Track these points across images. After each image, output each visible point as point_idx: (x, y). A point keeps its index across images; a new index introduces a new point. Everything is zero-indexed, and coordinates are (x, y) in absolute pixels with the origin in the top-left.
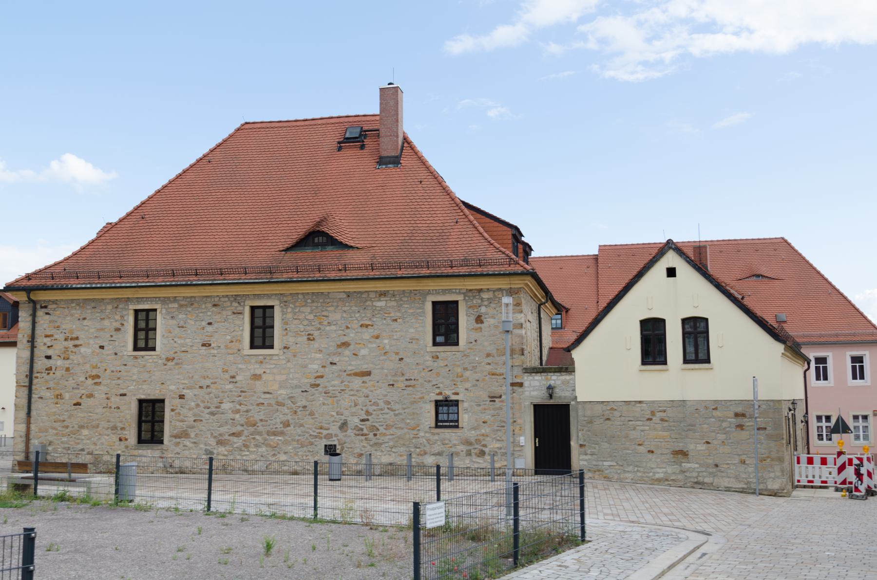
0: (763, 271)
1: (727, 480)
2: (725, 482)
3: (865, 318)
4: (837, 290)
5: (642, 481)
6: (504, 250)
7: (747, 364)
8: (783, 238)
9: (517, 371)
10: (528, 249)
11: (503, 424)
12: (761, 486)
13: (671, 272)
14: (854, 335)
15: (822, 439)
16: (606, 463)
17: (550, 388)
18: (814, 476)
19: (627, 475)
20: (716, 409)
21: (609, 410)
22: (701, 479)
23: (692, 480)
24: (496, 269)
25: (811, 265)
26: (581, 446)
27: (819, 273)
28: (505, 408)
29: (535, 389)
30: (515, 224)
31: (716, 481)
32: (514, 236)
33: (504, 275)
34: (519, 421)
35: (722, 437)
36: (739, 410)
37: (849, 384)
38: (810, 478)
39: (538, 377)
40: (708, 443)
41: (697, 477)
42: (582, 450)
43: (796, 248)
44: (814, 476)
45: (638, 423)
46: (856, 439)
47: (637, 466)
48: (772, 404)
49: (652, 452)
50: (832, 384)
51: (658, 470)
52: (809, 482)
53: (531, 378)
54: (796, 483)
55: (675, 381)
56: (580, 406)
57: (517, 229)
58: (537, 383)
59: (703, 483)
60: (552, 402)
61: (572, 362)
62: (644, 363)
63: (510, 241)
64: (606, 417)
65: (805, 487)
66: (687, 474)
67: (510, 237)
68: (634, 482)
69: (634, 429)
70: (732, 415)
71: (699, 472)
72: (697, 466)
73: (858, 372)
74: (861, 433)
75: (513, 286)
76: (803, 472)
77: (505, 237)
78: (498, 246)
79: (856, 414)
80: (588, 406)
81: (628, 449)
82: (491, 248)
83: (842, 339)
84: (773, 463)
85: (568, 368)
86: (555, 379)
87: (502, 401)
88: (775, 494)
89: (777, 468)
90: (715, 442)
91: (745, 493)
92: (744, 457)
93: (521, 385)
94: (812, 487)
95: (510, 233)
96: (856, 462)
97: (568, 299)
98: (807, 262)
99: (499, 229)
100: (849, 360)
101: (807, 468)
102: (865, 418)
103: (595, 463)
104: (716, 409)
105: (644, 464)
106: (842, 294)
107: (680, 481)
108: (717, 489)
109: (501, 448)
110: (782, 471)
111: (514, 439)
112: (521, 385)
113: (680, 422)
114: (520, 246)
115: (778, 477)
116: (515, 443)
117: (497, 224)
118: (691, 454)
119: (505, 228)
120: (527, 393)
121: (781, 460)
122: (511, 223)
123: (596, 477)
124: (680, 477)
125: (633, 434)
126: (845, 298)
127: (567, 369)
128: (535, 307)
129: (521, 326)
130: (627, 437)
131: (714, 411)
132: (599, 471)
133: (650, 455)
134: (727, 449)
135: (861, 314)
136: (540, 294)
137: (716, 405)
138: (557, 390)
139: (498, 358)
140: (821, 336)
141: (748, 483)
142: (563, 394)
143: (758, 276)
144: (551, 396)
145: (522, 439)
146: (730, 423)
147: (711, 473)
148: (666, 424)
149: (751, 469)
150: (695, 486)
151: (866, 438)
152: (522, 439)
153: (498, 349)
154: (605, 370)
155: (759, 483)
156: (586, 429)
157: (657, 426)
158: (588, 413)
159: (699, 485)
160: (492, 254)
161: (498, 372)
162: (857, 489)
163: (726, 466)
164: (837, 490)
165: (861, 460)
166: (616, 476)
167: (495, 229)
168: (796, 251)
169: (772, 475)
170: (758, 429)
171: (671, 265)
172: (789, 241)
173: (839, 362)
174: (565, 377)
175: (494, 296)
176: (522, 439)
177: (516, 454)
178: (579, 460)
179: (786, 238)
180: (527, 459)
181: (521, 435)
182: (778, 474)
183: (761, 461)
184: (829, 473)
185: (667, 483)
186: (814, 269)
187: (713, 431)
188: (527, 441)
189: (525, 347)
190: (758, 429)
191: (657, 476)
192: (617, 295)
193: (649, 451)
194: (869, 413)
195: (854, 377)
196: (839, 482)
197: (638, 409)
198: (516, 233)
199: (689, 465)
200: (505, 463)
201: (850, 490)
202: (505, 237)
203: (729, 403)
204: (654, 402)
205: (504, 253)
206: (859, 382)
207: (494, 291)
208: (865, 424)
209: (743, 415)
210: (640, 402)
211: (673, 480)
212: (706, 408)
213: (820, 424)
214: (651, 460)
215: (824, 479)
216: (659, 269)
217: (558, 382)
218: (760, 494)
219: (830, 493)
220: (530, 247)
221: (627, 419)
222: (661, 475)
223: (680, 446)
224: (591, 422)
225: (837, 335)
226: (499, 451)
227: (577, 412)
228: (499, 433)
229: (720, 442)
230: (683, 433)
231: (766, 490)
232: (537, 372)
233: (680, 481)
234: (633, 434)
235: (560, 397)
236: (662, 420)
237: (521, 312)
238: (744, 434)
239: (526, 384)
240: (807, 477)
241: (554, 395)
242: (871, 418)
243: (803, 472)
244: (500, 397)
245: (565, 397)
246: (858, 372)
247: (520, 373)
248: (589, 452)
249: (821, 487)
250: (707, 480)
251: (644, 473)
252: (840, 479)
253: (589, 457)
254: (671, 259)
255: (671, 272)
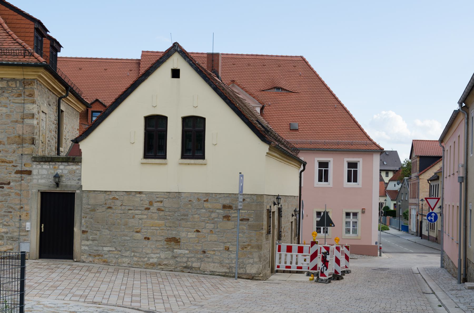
0: (283, 84)
1: (213, 264)
2: (211, 267)
3: (362, 130)
4: (342, 105)
5: (137, 265)
6: (20, 41)
7: (237, 160)
8: (302, 57)
9: (27, 159)
10: (56, 46)
11: (10, 210)
12: (241, 271)
13: (176, 73)
14: (352, 144)
15: (320, 232)
16: (105, 249)
17: (57, 177)
18: (291, 263)
19: (124, 260)
20: (207, 201)
21: (111, 199)
22: (189, 264)
23: (182, 265)
24: (11, 59)
25: (323, 82)
26: (84, 232)
27: (328, 89)
28: (13, 195)
29: (42, 177)
30: (38, 18)
31: (203, 266)
32: (37, 29)
33: (18, 65)
34: (26, 207)
35: (210, 226)
36: (227, 202)
37: (331, 185)
38: (288, 264)
39: (46, 166)
40: (198, 231)
41: (186, 262)
42: (84, 236)
43: (312, 66)
44: (291, 263)
45: (137, 212)
46: (346, 233)
47: (134, 252)
48: (255, 198)
49: (148, 239)
50: (331, 185)
51: (153, 255)
52: (287, 267)
53: (40, 166)
54: (276, 269)
55: (174, 175)
56: (84, 195)
57: (39, 22)
58: (45, 172)
59: (191, 268)
60: (58, 190)
61: (79, 153)
62: (146, 157)
63: (33, 35)
64: (108, 206)
65: (284, 272)
66: (178, 259)
67: (33, 30)
68: (131, 266)
69: (133, 217)
70: (221, 206)
71: (188, 258)
72: (187, 252)
73: (352, 176)
74: (351, 228)
75: (26, 77)
76: (283, 260)
77: (27, 30)
78: (15, 36)
79: (348, 211)
80: (92, 195)
81: (127, 236)
82: (9, 39)
83: (341, 147)
84: (252, 250)
85: (74, 157)
86: (63, 169)
87: (10, 188)
88: (252, 278)
89: (256, 255)
90: (204, 231)
91: (227, 276)
92: (228, 245)
93: (29, 173)
94: (290, 272)
95: (33, 26)
96: (324, 250)
97: (89, 97)
98: (320, 79)
99: (23, 22)
100: (346, 165)
101: (286, 255)
102: (355, 214)
103: (95, 248)
104: (207, 201)
105: (141, 250)
106: (345, 109)
107: (171, 266)
108: (203, 273)
109: (7, 233)
110: (260, 257)
111: (20, 225)
112: (29, 173)
113: (175, 212)
114: (46, 42)
115: (256, 263)
116: (21, 228)
117: (20, 17)
118: (182, 241)
119: (28, 21)
120: (35, 181)
121: (259, 247)
122: (35, 16)
123: (96, 261)
124: (172, 262)
125: (132, 222)
126: (348, 112)
127: (74, 159)
128: (53, 100)
129: (33, 116)
130: (126, 224)
131: (205, 203)
132: (99, 255)
133: (146, 242)
134: (214, 237)
135: (359, 127)
136: (59, 88)
137: (208, 197)
138: (64, 179)
139: (8, 146)
140: (325, 144)
141: (230, 268)
142: (69, 183)
143: (278, 88)
144: (57, 185)
145: (28, 224)
146: (219, 214)
147: (198, 259)
148: (162, 213)
149: (233, 256)
150: (185, 270)
151: (355, 231)
152: (28, 225)
153: (8, 138)
154: (110, 161)
155: (240, 268)
156: (89, 216)
157: (154, 215)
158: (92, 202)
159: (188, 269)
160: (8, 44)
161: (8, 159)
162: (323, 274)
163: (212, 253)
164: (309, 274)
165: (327, 249)
166: (114, 261)
167: (18, 21)
168: (312, 69)
169: (251, 261)
170: (241, 220)
171: (176, 67)
172: (307, 60)
173: (338, 166)
174: (73, 167)
175: (8, 85)
176: (28, 224)
177: (22, 238)
178: (81, 245)
179: (305, 57)
180: (31, 245)
181: (27, 221)
182: (256, 260)
183: (243, 249)
184: (303, 261)
185: (160, 267)
186: (325, 85)
187: (204, 221)
188: (32, 226)
189: (36, 137)
190: (241, 220)
191: (151, 261)
192: (125, 92)
193: (145, 238)
194: (359, 211)
195: (349, 181)
196: (310, 268)
197: (138, 199)
198: (40, 29)
199: (180, 251)
200: (11, 247)
201: (317, 276)
202: (27, 30)
203: (218, 196)
204: (152, 193)
205: (20, 44)
206: (352, 184)
207: (8, 81)
208: (355, 220)
209: (230, 207)
210: (140, 193)
211: (165, 264)
212: (199, 200)
213: (348, 220)
214: (146, 246)
215: (299, 265)
216: (164, 71)
217: (65, 172)
218: (239, 277)
219: (303, 278)
220: (58, 43)
221: (127, 208)
222: (155, 260)
223: (173, 234)
224: (94, 210)
225: (338, 144)
226: (5, 236)
227: (81, 200)
228: (6, 219)
229: (208, 231)
230: (177, 222)
231: (245, 274)
232: (45, 161)
233: (171, 266)
234: (132, 222)
235: (66, 186)
236: (159, 210)
237: (34, 102)
238: (230, 224)
239: (35, 172)
240: (286, 263)
241: (61, 183)
242: (360, 215)
243: (283, 260)
244: (9, 183)
245: (71, 186)
246: (352, 176)
247: (30, 161)
248: (90, 238)
249: (297, 272)
250: (195, 265)
251: (140, 257)
252: (312, 265)
253: (90, 242)
254: (176, 61)
255: (176, 73)
